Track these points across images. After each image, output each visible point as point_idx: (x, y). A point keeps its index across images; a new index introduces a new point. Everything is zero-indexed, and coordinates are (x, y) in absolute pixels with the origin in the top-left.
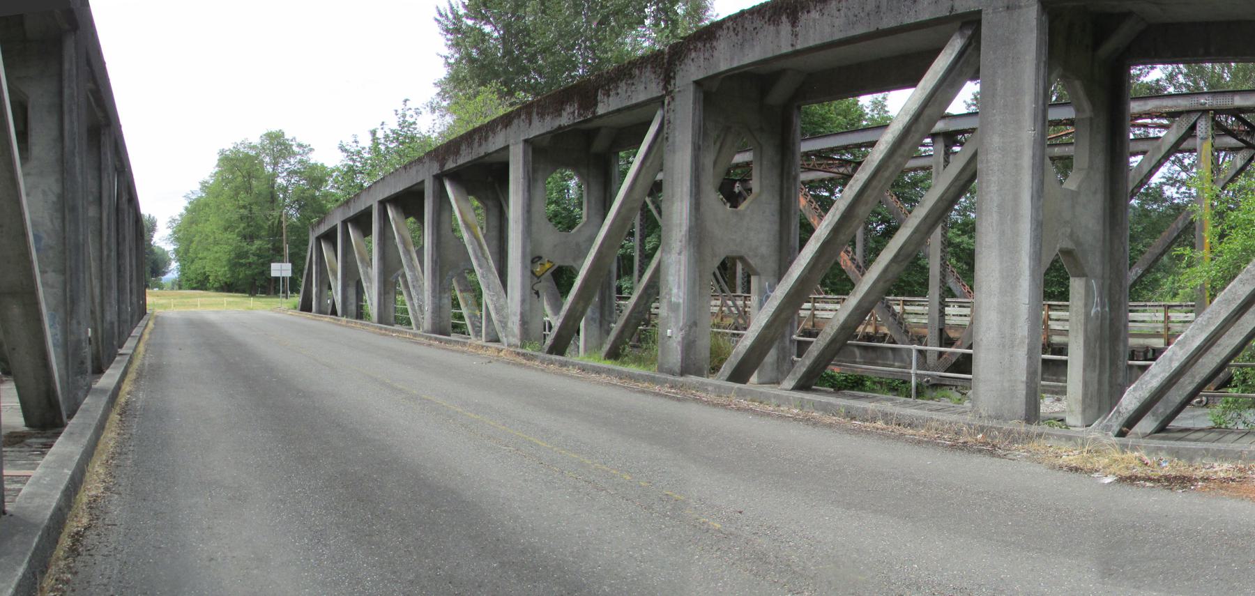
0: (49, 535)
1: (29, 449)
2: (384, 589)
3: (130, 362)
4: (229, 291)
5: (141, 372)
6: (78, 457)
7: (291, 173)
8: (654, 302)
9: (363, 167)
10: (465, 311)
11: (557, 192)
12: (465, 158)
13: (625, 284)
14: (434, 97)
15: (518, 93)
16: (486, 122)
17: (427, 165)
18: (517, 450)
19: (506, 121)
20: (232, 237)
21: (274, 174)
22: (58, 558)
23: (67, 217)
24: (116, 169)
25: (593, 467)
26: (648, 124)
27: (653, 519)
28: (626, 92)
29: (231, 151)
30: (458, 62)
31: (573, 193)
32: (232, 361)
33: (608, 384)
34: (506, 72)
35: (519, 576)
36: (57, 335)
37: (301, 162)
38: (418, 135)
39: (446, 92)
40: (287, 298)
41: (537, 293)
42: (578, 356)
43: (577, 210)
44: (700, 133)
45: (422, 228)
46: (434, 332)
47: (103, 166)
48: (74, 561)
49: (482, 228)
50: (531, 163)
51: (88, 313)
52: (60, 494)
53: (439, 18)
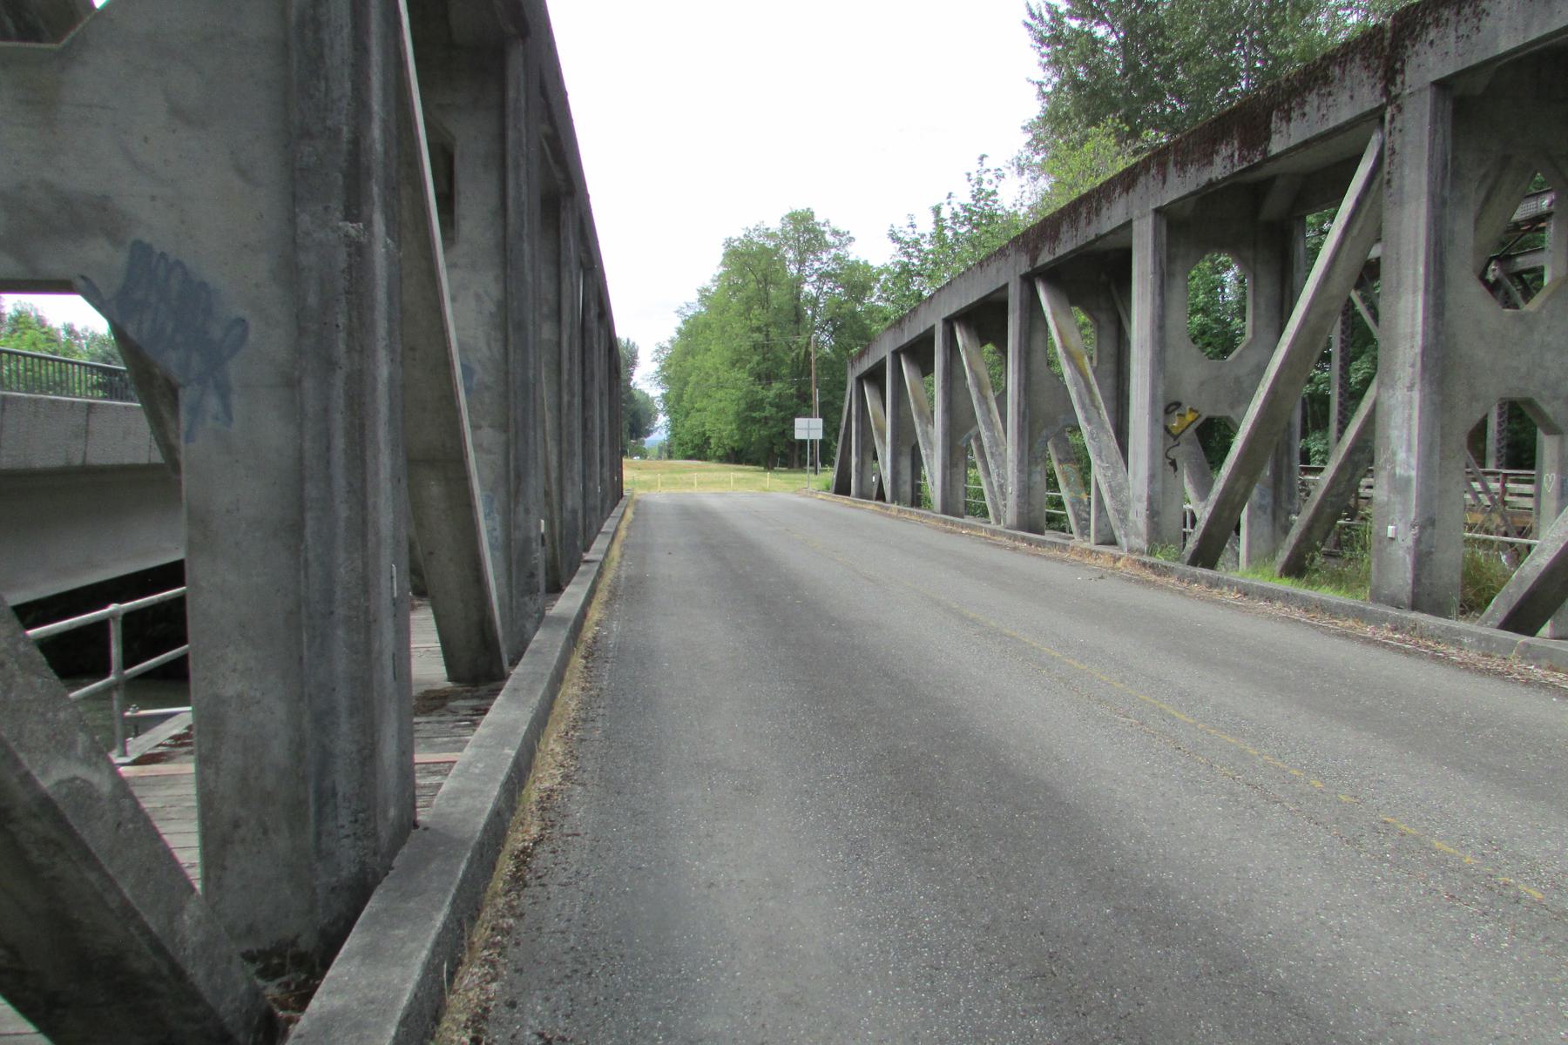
0: (482, 855)
1: (454, 718)
2: (949, 938)
3: (600, 574)
4: (738, 462)
5: (615, 589)
6: (525, 728)
7: (824, 276)
8: (1365, 476)
9: (922, 265)
10: (1065, 494)
11: (1205, 294)
12: (1067, 244)
13: (1315, 446)
14: (1022, 149)
15: (1145, 132)
16: (1098, 184)
17: (1011, 260)
18: (1142, 724)
19: (1128, 180)
20: (742, 376)
21: (800, 278)
22: (496, 893)
23: (511, 339)
24: (582, 264)
25: (1260, 760)
26: (1356, 160)
27: (1361, 863)
28: (1319, 108)
29: (742, 242)
30: (1058, 89)
31: (1230, 293)
32: (741, 572)
33: (1287, 619)
34: (1128, 99)
35: (1143, 933)
36: (495, 530)
37: (836, 258)
38: (999, 212)
39: (1039, 141)
40: (816, 473)
41: (1173, 463)
42: (1237, 571)
43: (1237, 320)
44: (1443, 179)
45: (1004, 361)
46: (1020, 527)
47: (563, 259)
48: (519, 896)
49: (1091, 359)
50: (1165, 248)
51: (541, 495)
52: (498, 789)
53: (1029, 20)
